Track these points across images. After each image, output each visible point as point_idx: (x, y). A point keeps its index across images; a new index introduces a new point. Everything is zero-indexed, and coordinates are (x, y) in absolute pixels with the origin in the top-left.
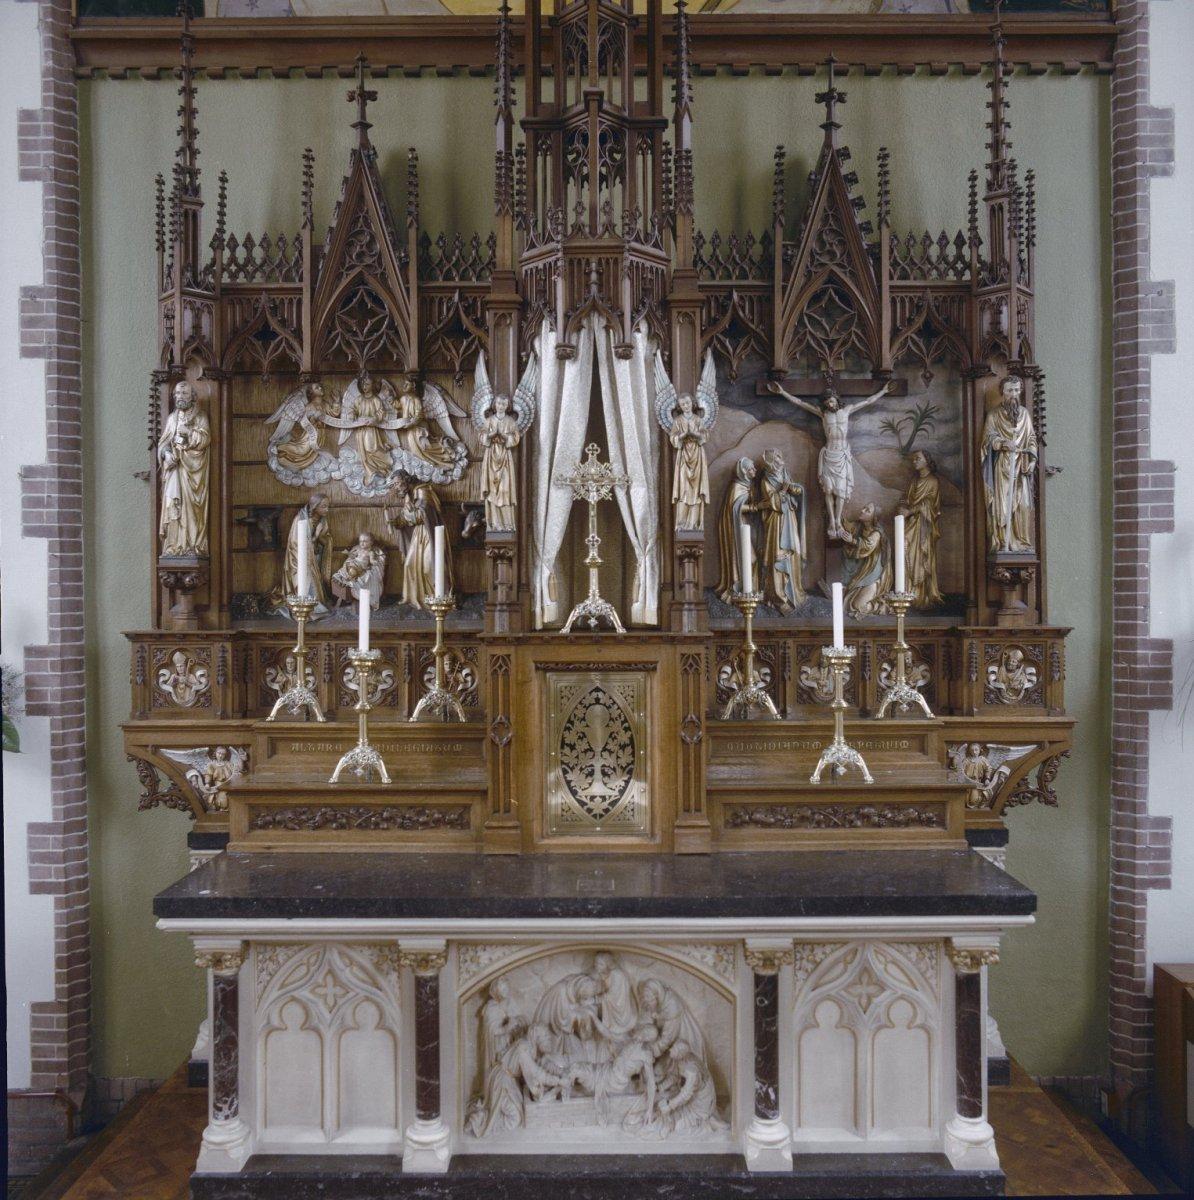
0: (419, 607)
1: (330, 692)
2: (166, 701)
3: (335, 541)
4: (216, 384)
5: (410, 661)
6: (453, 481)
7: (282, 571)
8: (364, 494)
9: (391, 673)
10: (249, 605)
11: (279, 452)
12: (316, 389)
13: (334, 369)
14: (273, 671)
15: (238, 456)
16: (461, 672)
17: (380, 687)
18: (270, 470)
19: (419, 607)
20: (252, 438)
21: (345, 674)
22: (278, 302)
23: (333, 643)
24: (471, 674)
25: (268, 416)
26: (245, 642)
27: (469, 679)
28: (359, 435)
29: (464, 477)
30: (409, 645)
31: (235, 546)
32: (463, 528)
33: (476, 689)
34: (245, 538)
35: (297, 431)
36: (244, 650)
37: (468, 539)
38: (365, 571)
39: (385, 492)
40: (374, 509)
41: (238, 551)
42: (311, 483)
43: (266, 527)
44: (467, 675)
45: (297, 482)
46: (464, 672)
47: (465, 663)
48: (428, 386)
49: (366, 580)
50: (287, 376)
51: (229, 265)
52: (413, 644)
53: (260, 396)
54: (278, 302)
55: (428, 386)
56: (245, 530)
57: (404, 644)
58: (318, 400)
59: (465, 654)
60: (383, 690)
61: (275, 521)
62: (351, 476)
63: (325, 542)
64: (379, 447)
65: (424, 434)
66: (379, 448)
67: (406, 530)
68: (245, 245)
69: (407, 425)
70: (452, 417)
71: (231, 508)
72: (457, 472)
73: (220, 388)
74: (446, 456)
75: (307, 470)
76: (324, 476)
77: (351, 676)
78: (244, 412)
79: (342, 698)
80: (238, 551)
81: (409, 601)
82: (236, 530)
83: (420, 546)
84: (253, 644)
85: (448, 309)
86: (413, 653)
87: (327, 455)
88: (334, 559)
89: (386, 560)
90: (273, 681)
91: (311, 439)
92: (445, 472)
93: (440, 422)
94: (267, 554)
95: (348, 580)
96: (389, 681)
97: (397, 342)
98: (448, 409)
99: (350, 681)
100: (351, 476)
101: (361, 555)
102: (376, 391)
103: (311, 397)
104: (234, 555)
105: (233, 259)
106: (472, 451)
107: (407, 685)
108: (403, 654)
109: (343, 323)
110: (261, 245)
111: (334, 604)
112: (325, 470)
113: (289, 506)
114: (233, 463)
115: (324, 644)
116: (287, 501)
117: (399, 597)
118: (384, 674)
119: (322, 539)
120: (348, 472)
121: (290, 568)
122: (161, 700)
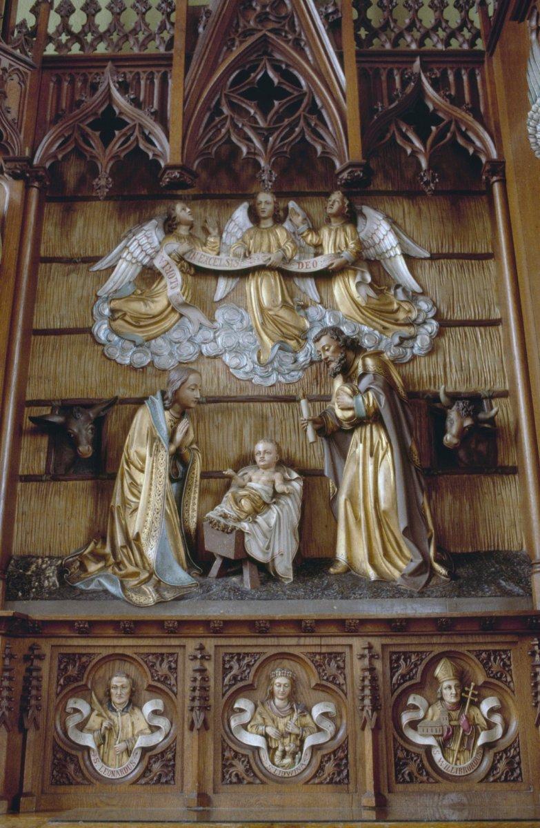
0: (372, 575)
1: (202, 753)
2: (249, 770)
3: (205, 462)
4: (19, 185)
5: (374, 679)
6: (414, 357)
7: (109, 512)
8: (257, 380)
9: (330, 708)
10: (40, 572)
11: (113, 311)
12: (182, 211)
13: (217, 179)
14: (84, 707)
15: (40, 323)
16: (477, 704)
17: (309, 742)
18: (96, 342)
19: (372, 575)
20: (69, 292)
21: (234, 711)
22: (129, 76)
23: (210, 644)
24: (500, 710)
25: (96, 259)
26: (28, 642)
27: (497, 719)
28: (251, 286)
29: (432, 350)
30: (370, 648)
31: (22, 471)
32: (444, 432)
33: (515, 744)
34: (43, 456)
35: (149, 275)
36: (27, 658)
37: (456, 448)
38: (267, 505)
39: (297, 375)
40: (276, 405)
41: (28, 479)
42: (165, 361)
43: (82, 429)
44: (492, 711)
45: (143, 359)
46: (485, 706)
47: (486, 685)
48: (367, 210)
49: (273, 521)
50: (141, 191)
51: (58, 33)
52: (377, 643)
53: (91, 223)
54: (129, 76)
55: (367, 210)
56: (44, 442)
57: (358, 644)
58: (183, 230)
59: (486, 665)
60: (314, 748)
61: (99, 424)
62: (237, 350)
63: (189, 457)
64: (284, 301)
65: (364, 279)
66: (285, 304)
67: (335, 436)
68: (85, 8)
69: (337, 262)
70: (408, 258)
71: (22, 404)
72: (421, 342)
73: (27, 188)
74: (401, 316)
75: (160, 341)
76: (188, 351)
77: (246, 717)
78: (58, 254)
79: (226, 766)
80: (28, 479)
81: (350, 567)
82: (26, 442)
83: (370, 462)
84: (46, 647)
85: (404, 83)
86: (378, 665)
87: (195, 315)
88: (203, 492)
89: (305, 488)
90: (81, 727)
91: (173, 286)
92: (402, 339)
93: (388, 265)
94: (80, 484)
95: (239, 520)
96: (329, 727)
97: (321, 132)
98: (401, 244)
99: (245, 727)
100: (237, 350)
101: (258, 481)
102: (279, 218)
103: (170, 226)
104: (19, 485)
105: (65, 27)
106: (444, 309)
107: (368, 735)
108: (356, 668)
109: (232, 106)
110: (109, 8)
111: (205, 572)
112: (190, 340)
113: (124, 401)
114: (31, 332)
115: (191, 645)
116: (121, 393)
117: (331, 560)
118: (317, 711)
119: (185, 451)
120: (236, 341)
121: (125, 502)
122: (240, 767)
